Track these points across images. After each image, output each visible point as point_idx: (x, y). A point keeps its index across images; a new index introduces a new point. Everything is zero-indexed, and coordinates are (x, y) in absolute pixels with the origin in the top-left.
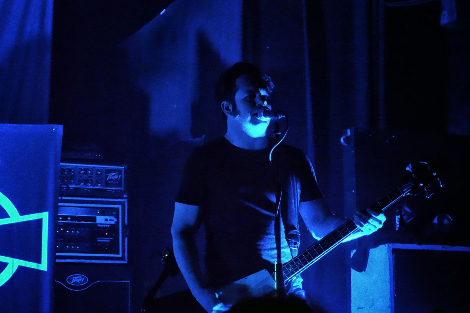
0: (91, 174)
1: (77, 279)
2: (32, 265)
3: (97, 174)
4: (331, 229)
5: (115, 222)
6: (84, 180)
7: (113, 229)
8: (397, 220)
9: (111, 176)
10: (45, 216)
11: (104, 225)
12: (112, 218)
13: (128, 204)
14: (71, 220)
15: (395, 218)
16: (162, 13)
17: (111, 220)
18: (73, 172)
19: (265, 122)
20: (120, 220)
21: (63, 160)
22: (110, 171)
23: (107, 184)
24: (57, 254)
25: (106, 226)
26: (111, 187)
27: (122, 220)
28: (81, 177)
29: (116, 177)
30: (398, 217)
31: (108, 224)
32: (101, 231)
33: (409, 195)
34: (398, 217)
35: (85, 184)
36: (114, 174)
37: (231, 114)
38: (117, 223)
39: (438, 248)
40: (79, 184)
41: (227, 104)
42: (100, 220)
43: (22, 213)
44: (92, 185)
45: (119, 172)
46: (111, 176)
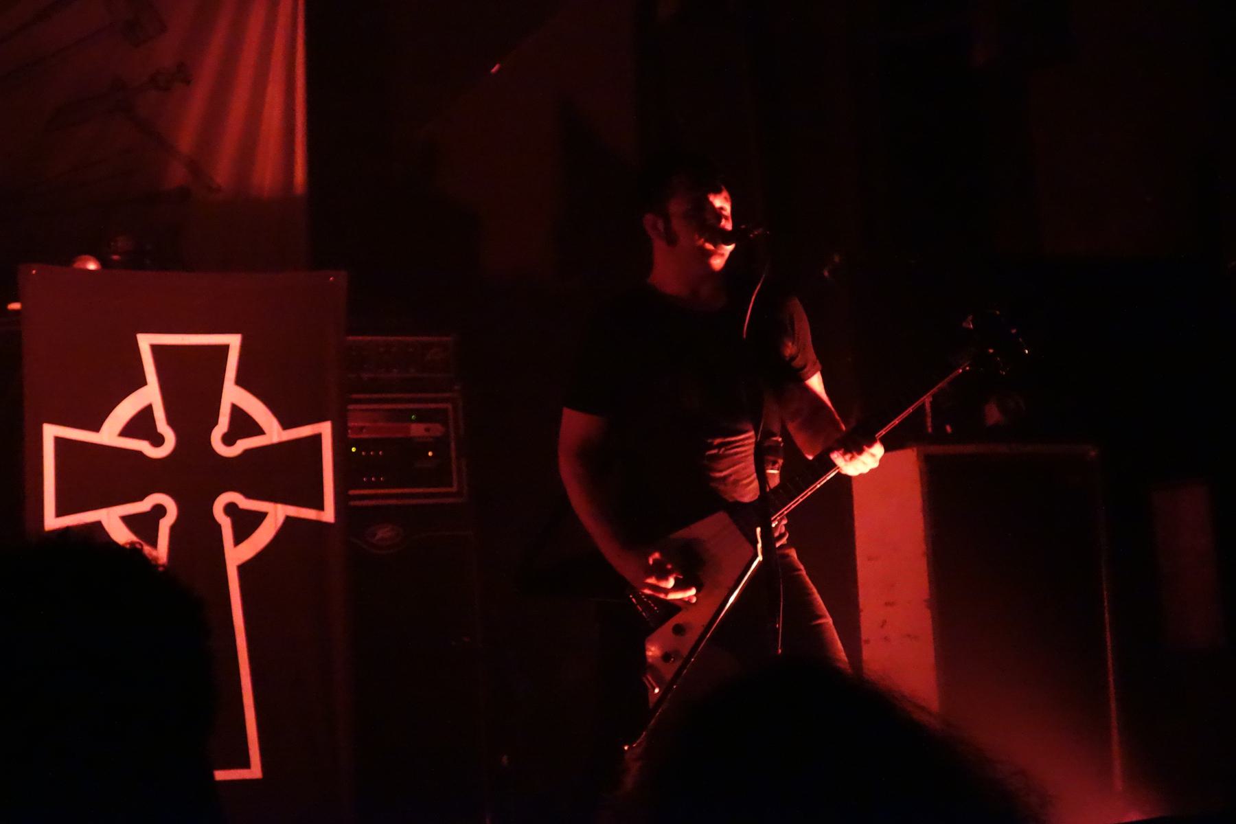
2: (309, 514)
7: (439, 444)
10: (325, 429)
17: (437, 429)
20: (411, 406)
24: (351, 492)
33: (645, 691)
43: (286, 425)
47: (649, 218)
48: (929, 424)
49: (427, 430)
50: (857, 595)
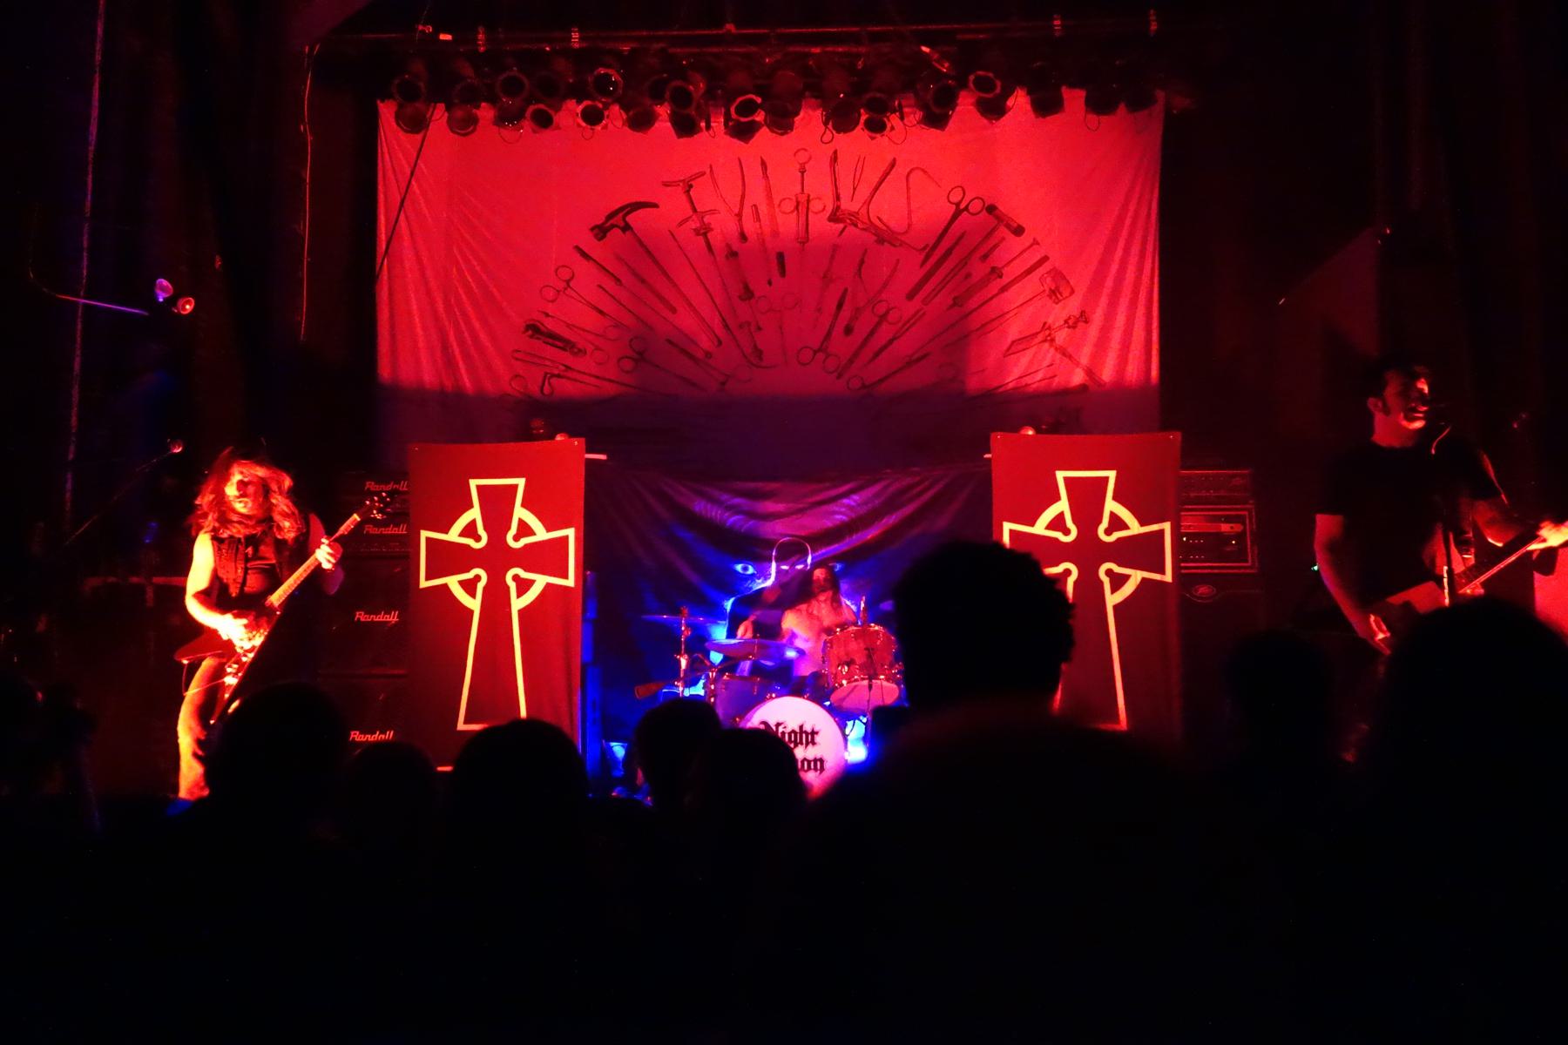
1: (1203, 590)
2: (1157, 577)
4: (1511, 536)
7: (1240, 537)
15: (1310, 526)
16: (602, 457)
17: (1238, 528)
22: (1234, 476)
32: (1226, 539)
38: (1244, 531)
42: (1225, 528)
43: (445, 586)
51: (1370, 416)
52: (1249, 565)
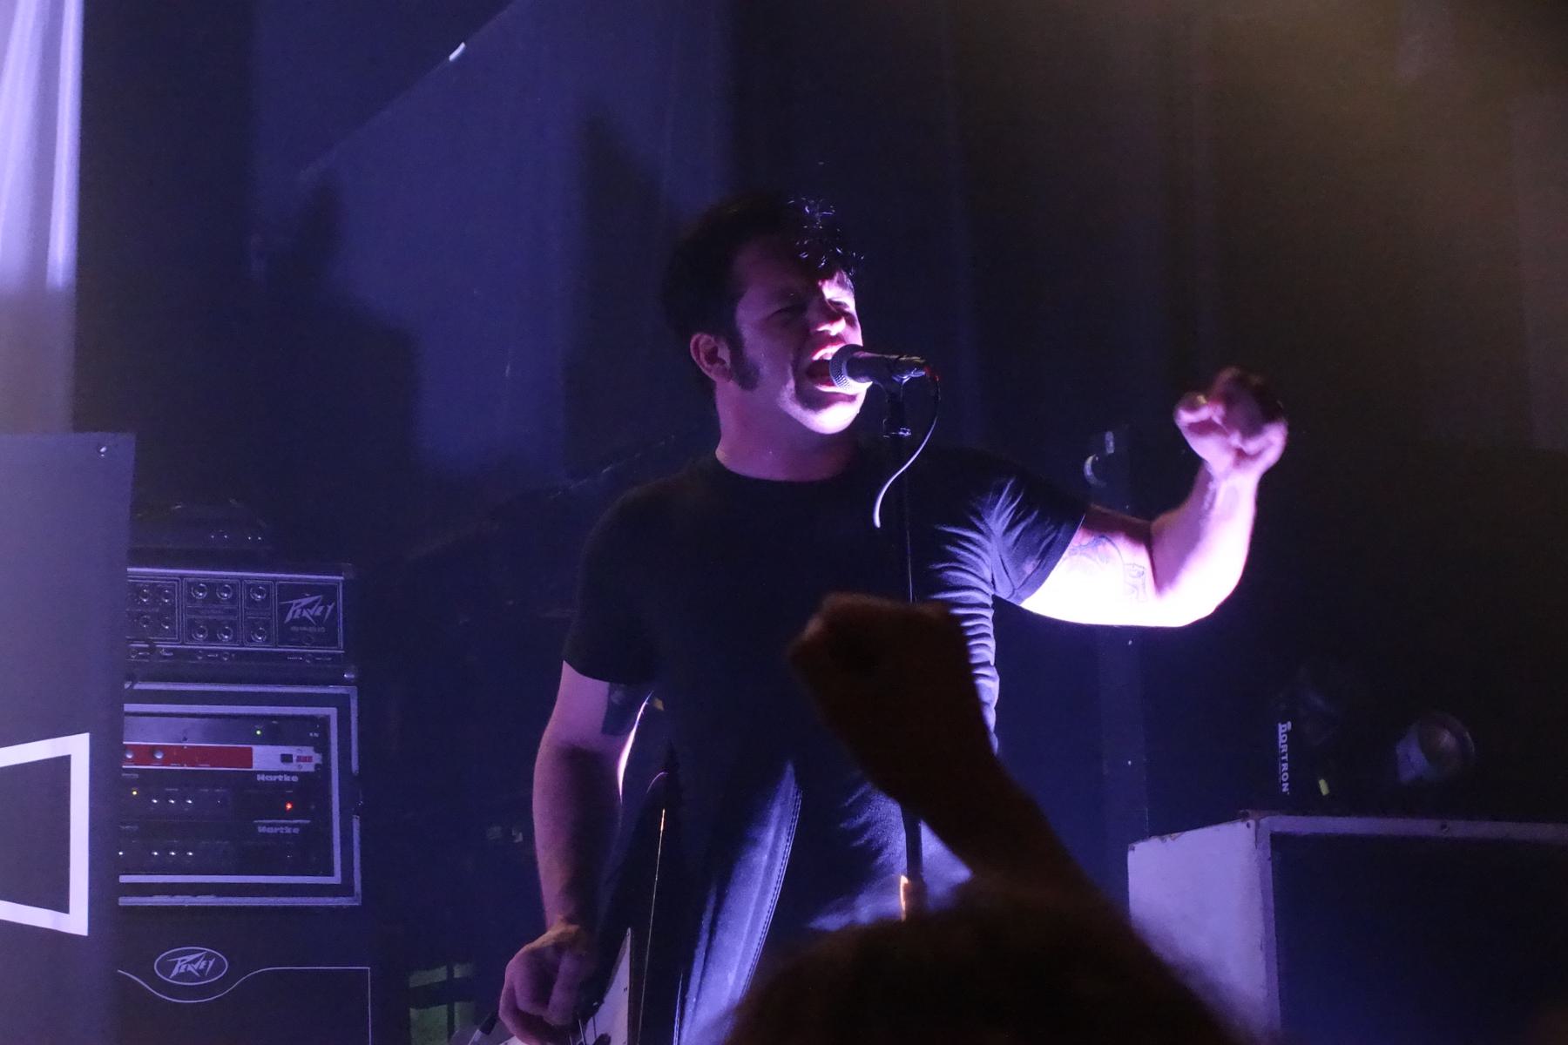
0: (232, 600)
1: (190, 963)
3: (251, 602)
5: (317, 766)
6: (207, 623)
7: (311, 788)
8: (1282, 739)
9: (299, 608)
10: (77, 748)
11: (280, 778)
12: (308, 751)
13: (359, 704)
14: (164, 762)
16: (453, 57)
17: (305, 759)
18: (167, 596)
19: (852, 398)
21: (139, 557)
22: (297, 591)
23: (285, 637)
24: (124, 879)
25: (287, 778)
26: (299, 644)
27: (336, 759)
28: (196, 611)
29: (318, 611)
30: (1283, 728)
31: (290, 774)
34: (1283, 728)
35: (212, 638)
36: (305, 601)
37: (727, 374)
38: (324, 768)
39: (1426, 827)
40: (191, 639)
41: (708, 342)
42: (265, 758)
44: (234, 640)
45: (328, 592)
46: (299, 608)
47: (701, 340)
48: (1285, 777)
49: (286, 758)
50: (717, 418)
51: (707, 387)
52: (334, 882)
